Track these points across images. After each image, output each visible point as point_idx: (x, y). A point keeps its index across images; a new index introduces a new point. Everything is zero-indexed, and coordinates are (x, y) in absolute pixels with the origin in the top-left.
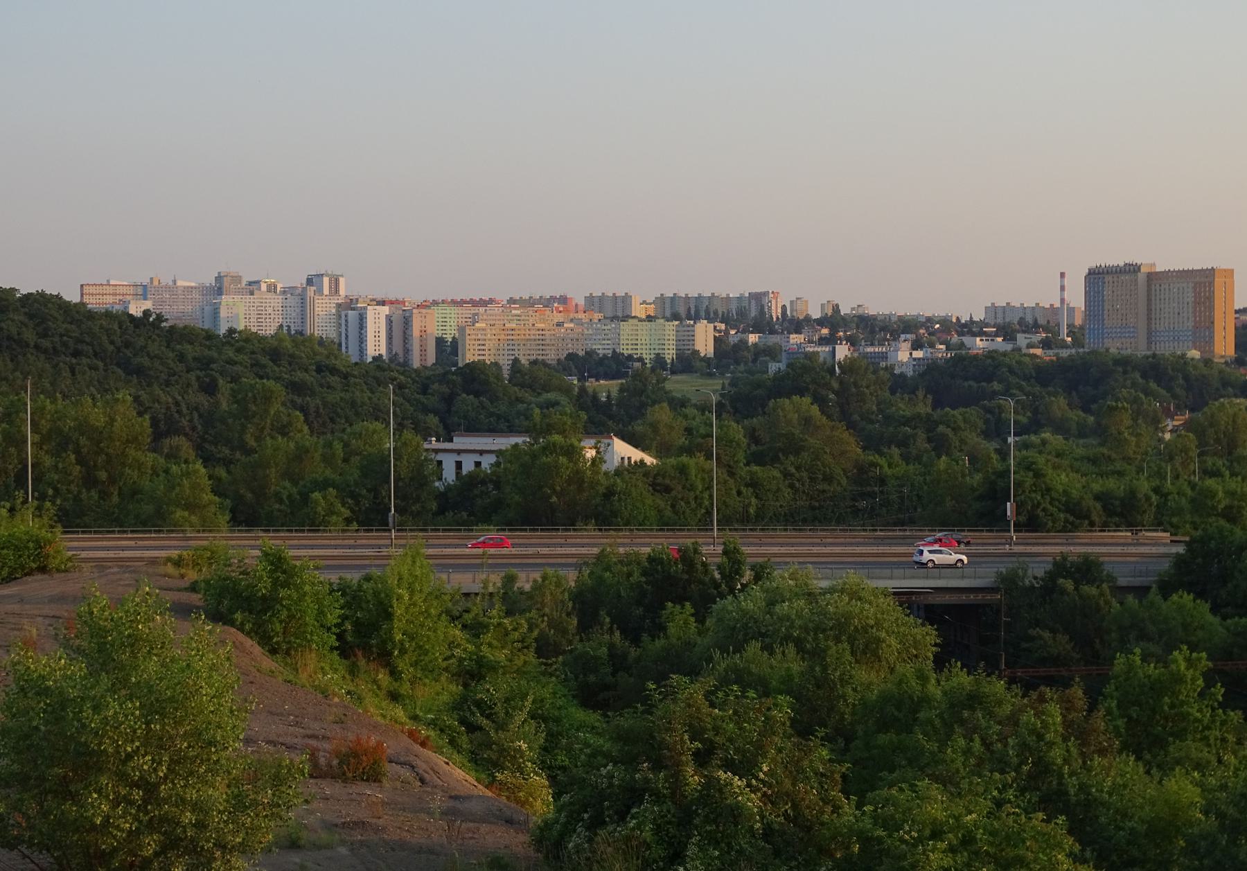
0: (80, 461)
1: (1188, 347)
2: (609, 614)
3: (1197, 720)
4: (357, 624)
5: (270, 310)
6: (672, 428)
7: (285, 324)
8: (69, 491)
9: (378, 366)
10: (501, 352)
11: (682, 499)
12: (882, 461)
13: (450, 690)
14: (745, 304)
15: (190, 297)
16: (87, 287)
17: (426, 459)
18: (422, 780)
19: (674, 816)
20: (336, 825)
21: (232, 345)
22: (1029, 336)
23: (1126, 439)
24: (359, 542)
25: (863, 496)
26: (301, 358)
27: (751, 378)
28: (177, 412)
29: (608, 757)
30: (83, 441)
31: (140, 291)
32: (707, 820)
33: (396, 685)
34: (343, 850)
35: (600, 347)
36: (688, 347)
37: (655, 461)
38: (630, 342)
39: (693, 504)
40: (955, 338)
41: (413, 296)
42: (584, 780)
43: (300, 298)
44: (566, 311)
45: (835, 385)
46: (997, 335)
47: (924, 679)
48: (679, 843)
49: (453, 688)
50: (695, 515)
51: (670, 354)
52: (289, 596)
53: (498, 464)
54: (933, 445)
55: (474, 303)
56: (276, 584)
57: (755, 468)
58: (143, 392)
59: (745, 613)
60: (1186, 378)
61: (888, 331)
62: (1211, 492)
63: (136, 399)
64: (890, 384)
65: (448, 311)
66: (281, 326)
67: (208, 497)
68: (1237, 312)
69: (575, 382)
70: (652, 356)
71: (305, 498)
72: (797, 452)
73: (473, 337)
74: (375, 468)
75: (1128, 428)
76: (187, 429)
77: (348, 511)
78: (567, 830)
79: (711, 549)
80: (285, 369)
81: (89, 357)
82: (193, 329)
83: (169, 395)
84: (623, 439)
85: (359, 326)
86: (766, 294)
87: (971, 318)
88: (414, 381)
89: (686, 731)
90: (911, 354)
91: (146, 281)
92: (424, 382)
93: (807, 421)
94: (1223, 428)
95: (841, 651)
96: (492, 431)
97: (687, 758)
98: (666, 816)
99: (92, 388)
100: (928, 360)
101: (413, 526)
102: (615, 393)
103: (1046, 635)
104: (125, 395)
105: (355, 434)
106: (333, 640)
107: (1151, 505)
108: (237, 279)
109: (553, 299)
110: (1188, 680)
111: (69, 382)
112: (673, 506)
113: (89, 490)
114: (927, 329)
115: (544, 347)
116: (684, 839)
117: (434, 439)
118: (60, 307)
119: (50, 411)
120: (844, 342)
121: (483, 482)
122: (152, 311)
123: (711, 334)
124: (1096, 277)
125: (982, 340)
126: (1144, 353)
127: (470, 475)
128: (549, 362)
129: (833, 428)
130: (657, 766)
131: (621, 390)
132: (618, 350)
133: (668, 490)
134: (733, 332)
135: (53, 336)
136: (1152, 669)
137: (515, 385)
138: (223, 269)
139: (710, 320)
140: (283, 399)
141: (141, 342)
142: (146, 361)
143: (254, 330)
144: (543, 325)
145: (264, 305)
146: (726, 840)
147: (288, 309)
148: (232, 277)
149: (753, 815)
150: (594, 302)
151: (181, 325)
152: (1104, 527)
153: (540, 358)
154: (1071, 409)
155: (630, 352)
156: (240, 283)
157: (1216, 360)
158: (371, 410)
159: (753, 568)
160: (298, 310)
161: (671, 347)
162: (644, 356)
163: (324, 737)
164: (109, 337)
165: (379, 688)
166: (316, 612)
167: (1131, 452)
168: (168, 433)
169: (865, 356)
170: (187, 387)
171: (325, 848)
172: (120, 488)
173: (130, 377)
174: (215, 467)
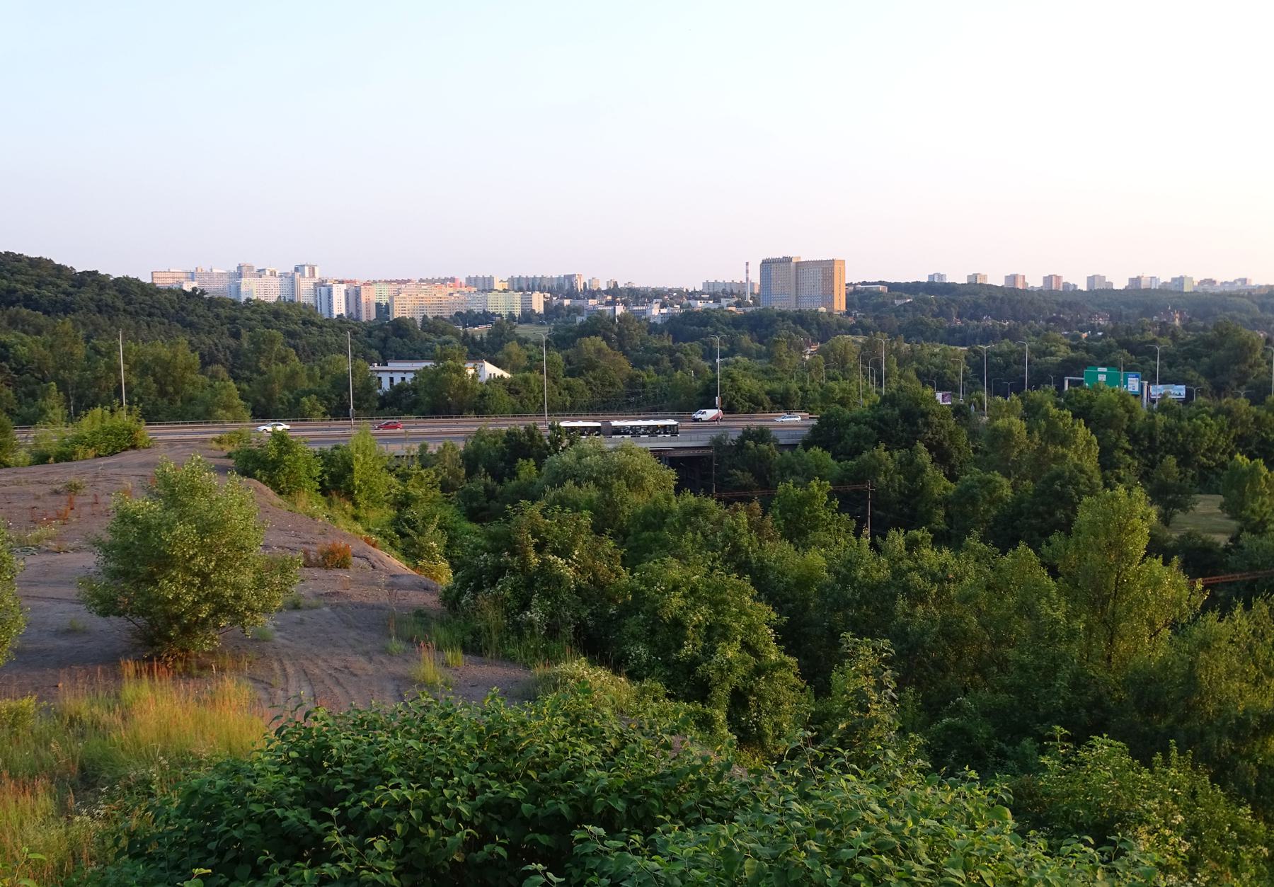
0: (155, 382)
3: (823, 520)
4: (332, 475)
12: (644, 374)
18: (373, 567)
25: (633, 394)
30: (158, 369)
31: (190, 275)
32: (543, 584)
33: (356, 511)
39: (533, 401)
41: (361, 278)
43: (291, 279)
44: (455, 286)
47: (668, 499)
49: (391, 512)
51: (517, 312)
53: (415, 379)
55: (398, 282)
56: (280, 452)
57: (569, 379)
59: (564, 463)
60: (818, 324)
63: (190, 342)
67: (237, 401)
71: (298, 401)
74: (340, 383)
78: (461, 593)
79: (543, 426)
84: (491, 363)
86: (574, 275)
91: (193, 270)
92: (370, 330)
93: (599, 351)
96: (411, 359)
97: (531, 548)
102: (485, 336)
103: (739, 473)
106: (317, 486)
108: (251, 268)
109: (446, 279)
112: (521, 402)
118: (138, 286)
121: (407, 390)
124: (767, 265)
127: (399, 386)
130: (513, 553)
133: (517, 392)
138: (242, 262)
141: (191, 307)
142: (195, 319)
143: (263, 299)
168: (210, 363)
169: (633, 312)
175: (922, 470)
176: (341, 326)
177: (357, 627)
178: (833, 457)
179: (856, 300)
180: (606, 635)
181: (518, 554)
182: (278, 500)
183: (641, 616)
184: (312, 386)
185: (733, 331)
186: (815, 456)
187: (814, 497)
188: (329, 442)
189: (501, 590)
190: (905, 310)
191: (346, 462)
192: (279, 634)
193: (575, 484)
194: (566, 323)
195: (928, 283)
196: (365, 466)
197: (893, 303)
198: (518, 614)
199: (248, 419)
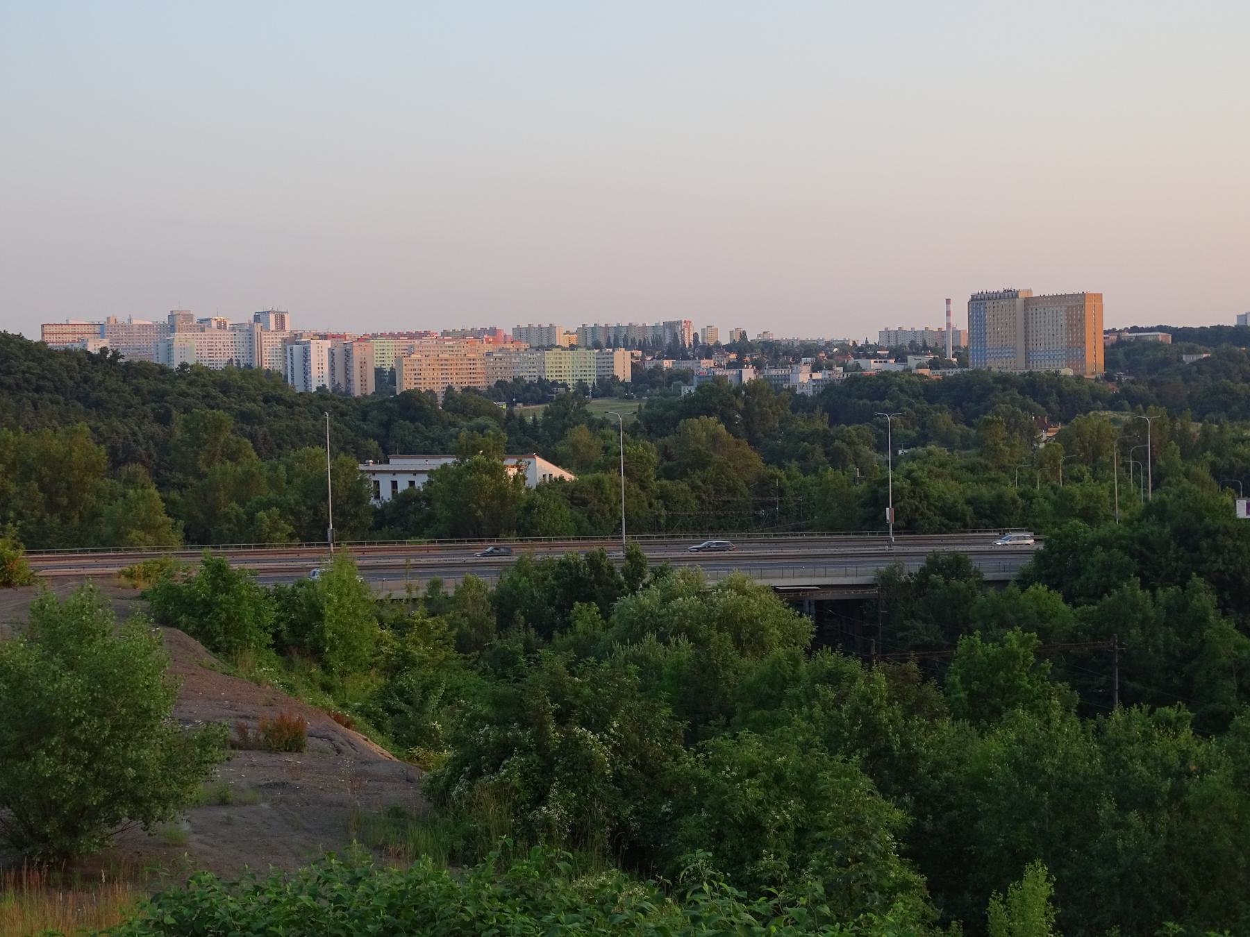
0: (42, 489)
1: (1062, 365)
2: (523, 613)
3: (1028, 691)
4: (292, 624)
5: (220, 346)
6: (590, 447)
7: (234, 358)
8: (33, 516)
9: (321, 396)
10: (436, 381)
11: (598, 511)
12: (781, 474)
13: (376, 681)
14: (660, 332)
15: (145, 334)
16: (48, 327)
17: (362, 479)
18: (339, 751)
19: (538, 765)
20: (260, 786)
21: (185, 379)
22: (917, 358)
23: (1001, 450)
24: (302, 556)
25: (764, 505)
26: (249, 389)
27: (665, 400)
28: (135, 441)
29: (486, 719)
30: (45, 471)
31: (98, 329)
32: (566, 769)
33: (328, 678)
34: (265, 806)
35: (526, 374)
36: (608, 373)
37: (573, 477)
38: (554, 369)
39: (608, 516)
40: (852, 361)
41: (353, 328)
42: (466, 739)
43: (249, 333)
44: (495, 341)
45: (741, 405)
46: (889, 357)
47: (796, 663)
48: (543, 788)
49: (381, 681)
50: (611, 525)
51: (591, 380)
52: (228, 600)
53: (430, 483)
54: (830, 458)
55: (410, 336)
56: (216, 589)
57: (665, 482)
58: (102, 424)
59: (642, 608)
60: (1060, 394)
61: (791, 355)
62: (1070, 495)
63: (95, 430)
64: (790, 403)
65: (386, 344)
66: (231, 360)
67: (162, 518)
68: (1106, 332)
69: (504, 407)
70: (575, 382)
71: (251, 518)
72: (703, 467)
73: (410, 367)
74: (314, 489)
75: (1003, 439)
76: (144, 457)
77: (291, 527)
78: (451, 781)
79: (615, 554)
80: (234, 400)
81: (51, 393)
82: (148, 364)
83: (127, 425)
84: (546, 458)
85: (303, 359)
87: (867, 342)
88: (355, 409)
89: (548, 695)
90: (811, 376)
91: (103, 320)
92: (363, 409)
93: (714, 438)
94: (1088, 437)
95: (723, 639)
96: (427, 453)
97: (550, 718)
98: (532, 765)
99: (54, 421)
100: (826, 381)
101: (351, 540)
102: (540, 417)
103: (920, 625)
104: (82, 426)
105: (298, 458)
106: (269, 639)
107: (1017, 508)
108: (189, 317)
109: (484, 330)
110: (1021, 657)
111: (31, 415)
112: (589, 518)
113: (52, 514)
114: (826, 353)
115: (474, 376)
116: (547, 785)
117: (371, 461)
118: (22, 346)
119: (13, 443)
120: (751, 366)
121: (417, 500)
122: (109, 348)
123: (629, 360)
124: (978, 303)
125: (875, 362)
126: (1022, 371)
127: (405, 493)
128: (480, 389)
129: (738, 444)
130: (524, 725)
131: (546, 413)
132: (543, 377)
133: (584, 503)
134: (649, 358)
135: (16, 373)
136: (992, 649)
137: (448, 411)
138: (175, 308)
139: (627, 348)
140: (232, 427)
141: (98, 377)
142: (104, 395)
143: (205, 364)
144: (474, 355)
145: (214, 341)
146: (582, 784)
147: (237, 344)
148: (184, 315)
149: (603, 763)
150: (521, 333)
151: (137, 361)
152: (976, 528)
153: (472, 385)
154: (955, 423)
155: (554, 378)
156: (192, 321)
157: (1086, 377)
158: (315, 435)
159: (653, 570)
160: (246, 345)
161: (592, 373)
162: (568, 382)
163: (254, 718)
164: (68, 373)
165: (312, 681)
166: (253, 614)
167: (1006, 461)
168: (125, 461)
169: (768, 379)
170: (143, 418)
171: (249, 804)
172: (80, 512)
173: (88, 410)
174: (169, 491)
175: (1202, 620)
176: (322, 403)
177: (305, 829)
178: (1066, 601)
179: (1120, 355)
180: (655, 843)
181: (531, 725)
182: (209, 659)
183: (704, 815)
184: (272, 495)
185: (925, 406)
186: (1036, 598)
187: (1013, 656)
188: (292, 578)
189: (505, 776)
190: (1199, 371)
191: (313, 605)
192: (195, 837)
193: (658, 639)
194: (666, 396)
195: (1236, 328)
196: (341, 610)
197: (1180, 360)
198: (530, 810)
199: (178, 545)
